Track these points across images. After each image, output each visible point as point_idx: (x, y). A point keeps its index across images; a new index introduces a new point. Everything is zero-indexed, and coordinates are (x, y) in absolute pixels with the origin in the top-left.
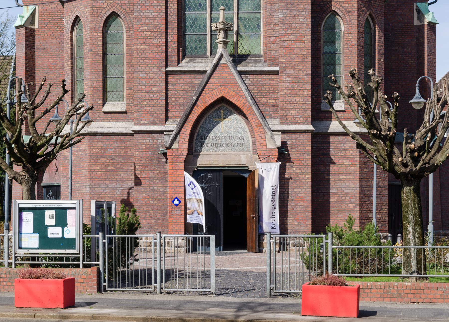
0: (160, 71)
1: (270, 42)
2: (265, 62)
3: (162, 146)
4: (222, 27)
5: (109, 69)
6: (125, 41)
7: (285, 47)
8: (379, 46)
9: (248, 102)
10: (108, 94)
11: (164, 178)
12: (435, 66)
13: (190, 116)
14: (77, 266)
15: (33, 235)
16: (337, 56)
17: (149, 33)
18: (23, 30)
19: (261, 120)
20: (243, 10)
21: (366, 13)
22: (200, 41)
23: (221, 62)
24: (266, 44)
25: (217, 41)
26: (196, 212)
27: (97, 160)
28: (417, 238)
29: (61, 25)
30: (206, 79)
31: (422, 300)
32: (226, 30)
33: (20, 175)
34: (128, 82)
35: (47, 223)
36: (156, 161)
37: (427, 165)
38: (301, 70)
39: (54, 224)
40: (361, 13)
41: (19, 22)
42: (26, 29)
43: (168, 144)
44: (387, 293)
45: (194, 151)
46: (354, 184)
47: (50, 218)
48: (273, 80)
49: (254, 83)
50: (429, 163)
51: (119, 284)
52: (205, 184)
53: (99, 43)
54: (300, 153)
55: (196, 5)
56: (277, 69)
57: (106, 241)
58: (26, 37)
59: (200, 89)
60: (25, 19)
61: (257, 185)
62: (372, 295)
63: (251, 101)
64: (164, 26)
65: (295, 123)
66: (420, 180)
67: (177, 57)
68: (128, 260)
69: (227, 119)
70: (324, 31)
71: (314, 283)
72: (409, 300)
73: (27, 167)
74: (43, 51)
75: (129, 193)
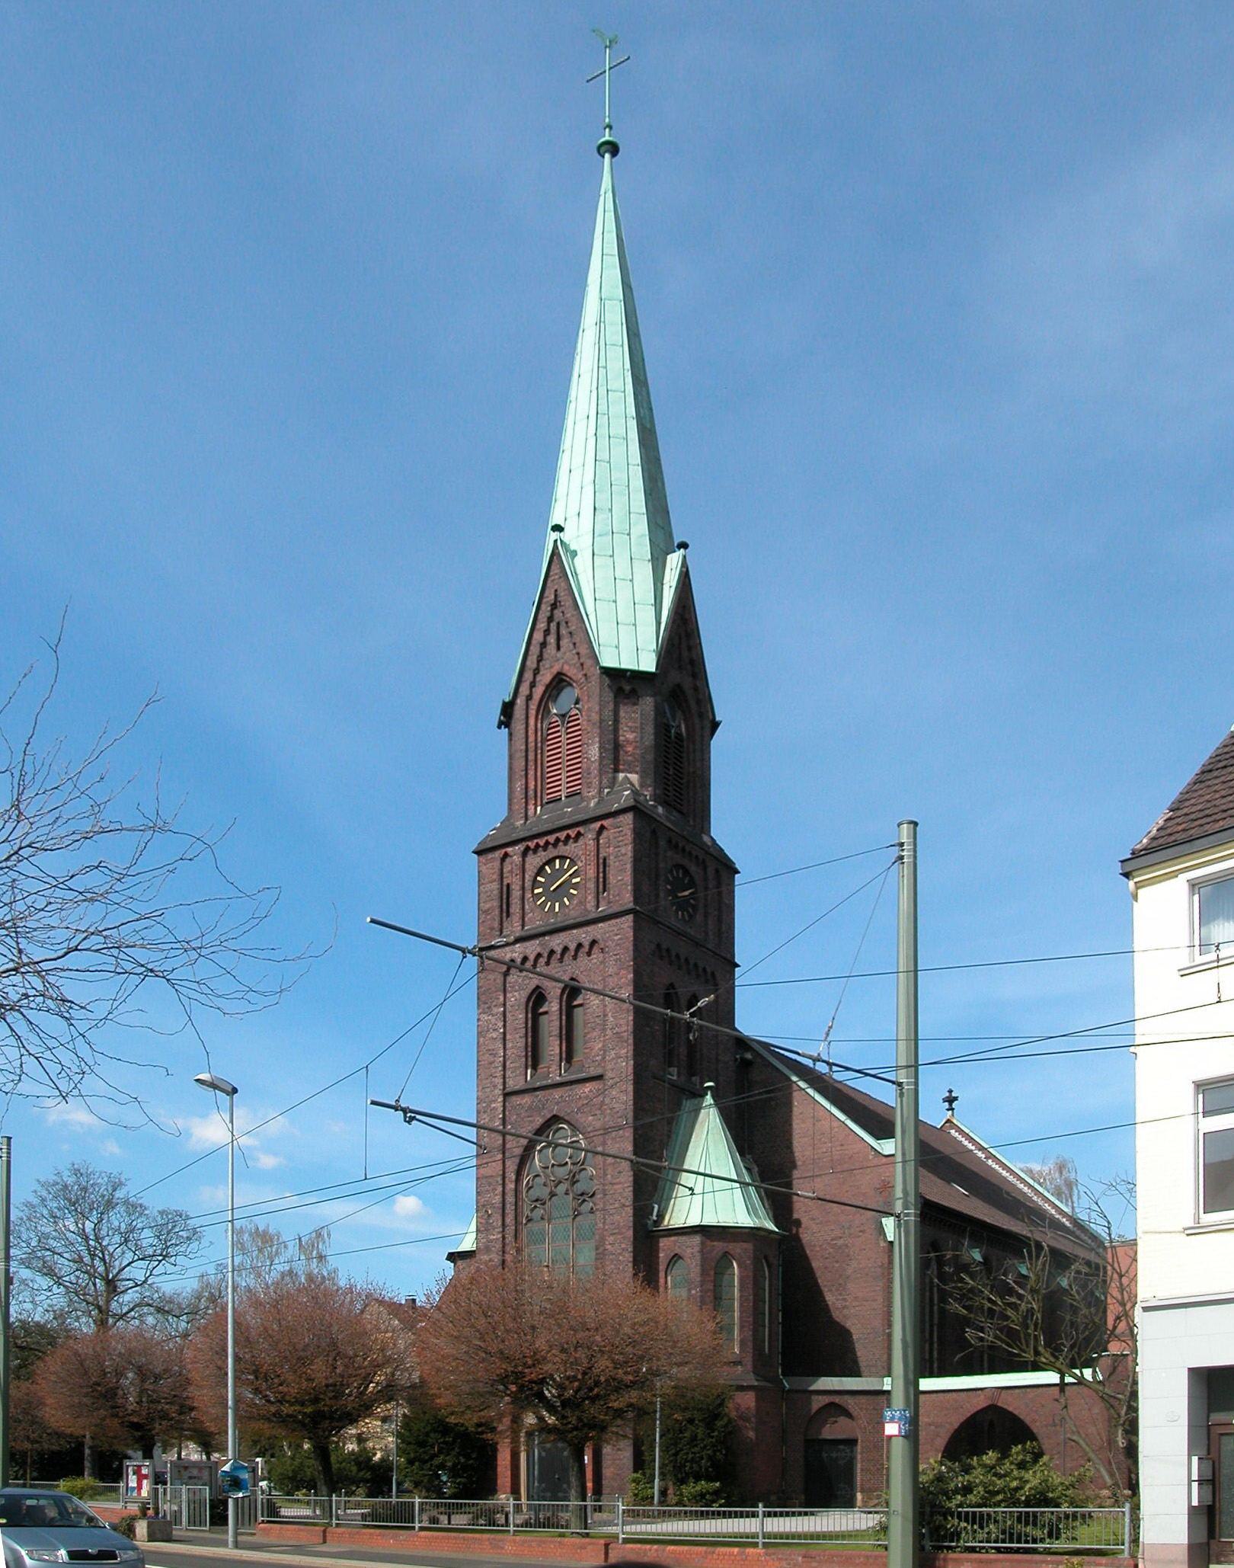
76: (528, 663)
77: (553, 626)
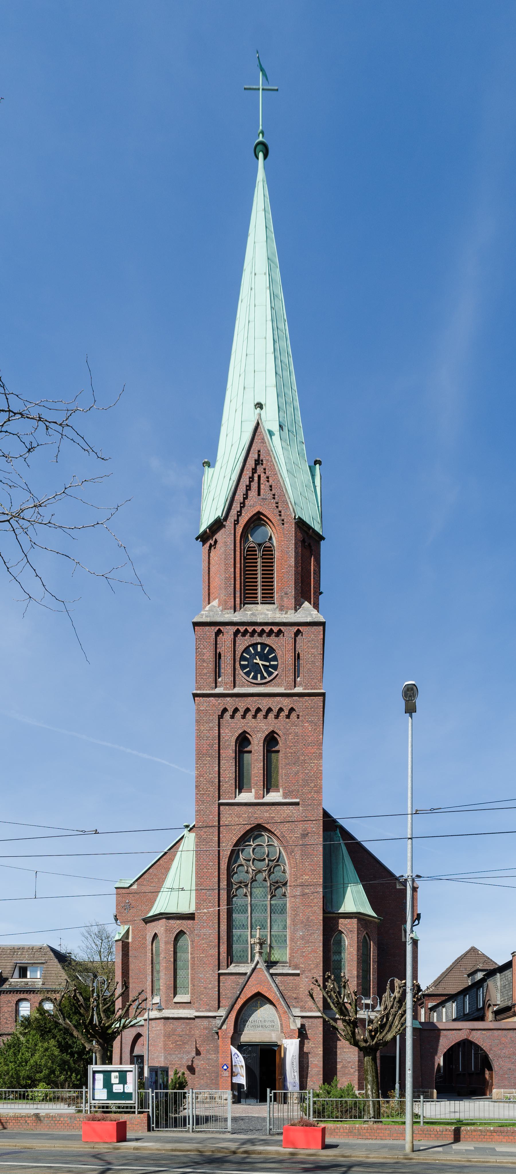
0: (214, 973)
1: (294, 953)
2: (289, 967)
3: (216, 1027)
4: (258, 941)
6: (190, 951)
7: (303, 956)
8: (373, 956)
9: (277, 995)
10: (178, 989)
11: (216, 1050)
12: (417, 971)
13: (235, 1006)
14: (134, 1112)
15: (103, 1090)
16: (343, 963)
17: (206, 945)
18: (120, 943)
19: (286, 1009)
20: (274, 929)
21: (363, 932)
22: (243, 951)
23: (257, 967)
24: (290, 954)
25: (254, 952)
27: (170, 1037)
28: (374, 1093)
29: (145, 938)
30: (247, 979)
31: (375, 1137)
32: (261, 944)
33: (95, 1047)
34: (192, 980)
36: (211, 1038)
37: (381, 1041)
38: (315, 973)
39: (118, 1082)
40: (360, 932)
41: (117, 937)
43: (219, 1026)
44: (351, 1132)
46: (354, 1055)
47: (115, 1078)
48: (295, 980)
49: (281, 982)
50: (382, 1040)
52: (246, 1054)
53: (171, 953)
54: (314, 1032)
55: (240, 925)
56: (298, 972)
57: (154, 1094)
58: (122, 948)
59: (242, 986)
62: (340, 1134)
63: (279, 995)
64: (217, 940)
65: (311, 1011)
66: (376, 1052)
68: (179, 1109)
69: (262, 1008)
70: (333, 945)
71: (292, 1125)
72: (366, 1137)
73: (99, 1041)
74: (134, 958)
75: (192, 1061)
76: (237, 497)
77: (256, 475)
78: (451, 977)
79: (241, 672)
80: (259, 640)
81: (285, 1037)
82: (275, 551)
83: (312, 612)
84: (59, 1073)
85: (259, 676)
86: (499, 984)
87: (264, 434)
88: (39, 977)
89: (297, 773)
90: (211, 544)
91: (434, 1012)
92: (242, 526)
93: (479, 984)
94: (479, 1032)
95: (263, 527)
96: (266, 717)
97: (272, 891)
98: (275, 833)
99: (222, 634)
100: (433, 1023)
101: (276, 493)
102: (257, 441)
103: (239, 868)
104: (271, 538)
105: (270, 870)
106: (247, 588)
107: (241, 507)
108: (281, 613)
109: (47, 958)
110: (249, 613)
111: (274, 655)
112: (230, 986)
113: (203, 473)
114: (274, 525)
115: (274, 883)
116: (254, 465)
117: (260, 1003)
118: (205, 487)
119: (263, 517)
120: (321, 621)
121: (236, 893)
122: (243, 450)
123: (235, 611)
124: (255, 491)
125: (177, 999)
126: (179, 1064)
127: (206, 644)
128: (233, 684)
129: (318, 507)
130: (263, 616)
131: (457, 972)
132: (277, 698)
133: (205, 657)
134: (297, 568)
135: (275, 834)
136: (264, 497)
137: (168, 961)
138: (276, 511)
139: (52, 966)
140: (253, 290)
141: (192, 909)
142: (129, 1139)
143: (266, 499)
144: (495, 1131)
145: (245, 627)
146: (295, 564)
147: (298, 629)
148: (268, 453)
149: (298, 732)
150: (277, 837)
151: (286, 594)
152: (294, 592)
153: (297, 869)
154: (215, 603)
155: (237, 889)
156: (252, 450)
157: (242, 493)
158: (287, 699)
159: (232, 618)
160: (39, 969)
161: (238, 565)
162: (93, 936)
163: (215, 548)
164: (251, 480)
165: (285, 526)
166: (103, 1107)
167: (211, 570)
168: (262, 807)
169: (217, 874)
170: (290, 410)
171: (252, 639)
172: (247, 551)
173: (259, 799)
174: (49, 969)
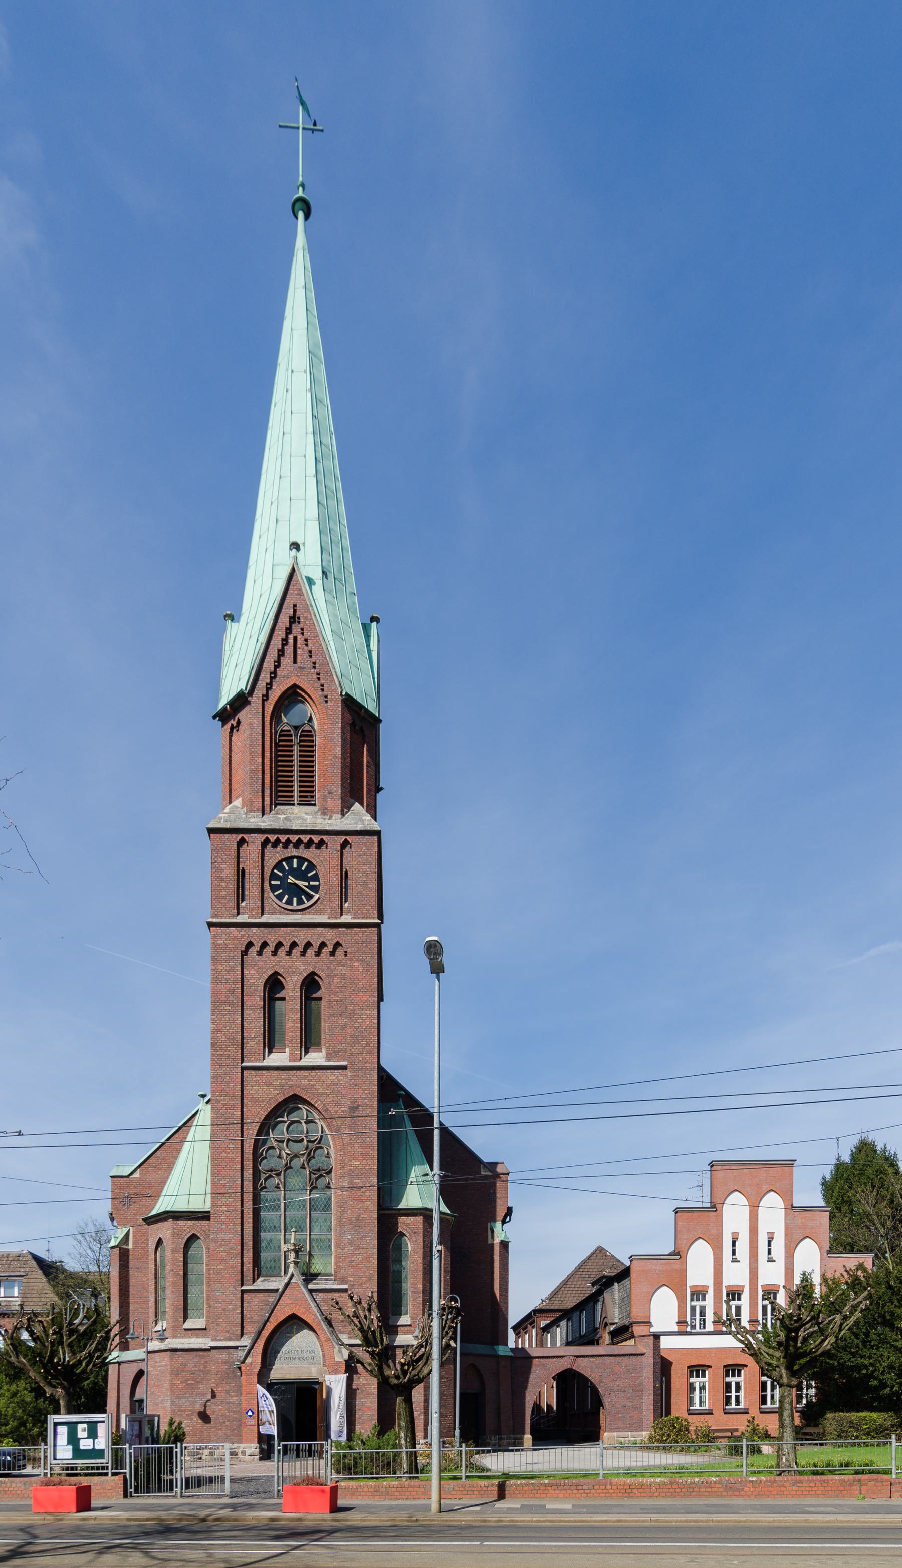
3: (238, 1361)
4: (292, 1247)
5: (190, 1288)
6: (205, 1261)
9: (318, 1318)
10: (189, 1312)
11: (239, 1390)
13: (263, 1332)
14: (106, 1474)
15: (66, 1447)
17: (225, 1254)
18: (117, 1251)
23: (292, 1281)
24: (336, 1263)
26: (267, 1423)
27: (178, 1374)
30: (278, 1297)
31: (407, 1497)
32: (297, 1251)
34: (207, 1300)
35: (79, 1436)
38: (368, 1288)
39: (86, 1436)
40: (427, 1233)
41: (113, 1243)
42: (120, 1249)
43: (241, 1359)
44: (377, 1491)
45: (267, 1364)
49: (324, 1300)
50: (418, 1375)
51: (155, 1490)
52: (279, 1395)
55: (270, 1227)
57: (132, 1451)
60: (119, 1240)
61: (324, 1396)
64: (239, 1247)
67: (252, 1276)
69: (299, 1334)
70: (393, 1250)
75: (205, 1406)
76: (265, 665)
77: (291, 637)
78: (571, 1286)
79: (271, 895)
80: (295, 853)
81: (328, 1373)
82: (315, 736)
83: (364, 818)
84: (31, 1425)
85: (295, 899)
86: (617, 1297)
87: (302, 584)
88: (16, 1295)
89: (344, 1028)
90: (232, 725)
91: (548, 1333)
92: (273, 703)
93: (593, 1299)
94: (586, 1359)
95: (300, 705)
96: (303, 953)
97: (313, 1182)
98: (316, 1105)
99: (246, 844)
100: (523, 1349)
101: (317, 661)
102: (292, 592)
103: (269, 1152)
104: (310, 719)
105: (310, 1153)
106: (279, 784)
107: (271, 678)
108: (324, 817)
109: (27, 1269)
110: (282, 817)
111: (314, 872)
112: (256, 1307)
113: (224, 630)
114: (314, 702)
115: (315, 1171)
116: (288, 624)
117: (296, 1329)
118: (227, 648)
119: (300, 692)
120: (376, 829)
121: (265, 1184)
122: (234, 640)
123: (263, 814)
124: (290, 657)
125: (187, 1325)
126: (190, 1410)
127: (226, 857)
128: (260, 911)
129: (374, 678)
130: (300, 822)
131: (578, 1279)
132: (318, 929)
133: (224, 875)
134: (345, 759)
135: (315, 1107)
136: (301, 666)
137: (176, 1275)
138: (317, 685)
139: (33, 1280)
140: (289, 392)
141: (207, 1207)
142: (95, 1508)
143: (304, 668)
144: (549, 1485)
145: (276, 836)
146: (342, 754)
147: (346, 840)
148: (307, 609)
149: (345, 974)
150: (318, 1110)
151: (330, 793)
152: (340, 791)
153: (344, 1152)
154: (237, 803)
155: (266, 1179)
156: (285, 603)
157: (273, 660)
158: (331, 931)
159: (259, 824)
160: (16, 1284)
161: (267, 754)
162: (88, 1239)
163: (237, 730)
164: (284, 642)
165: (328, 704)
166: (67, 1469)
167: (233, 758)
168: (298, 1071)
169: (239, 1159)
170: (337, 551)
171: (285, 851)
172: (280, 736)
173: (294, 1061)
174: (30, 1284)
